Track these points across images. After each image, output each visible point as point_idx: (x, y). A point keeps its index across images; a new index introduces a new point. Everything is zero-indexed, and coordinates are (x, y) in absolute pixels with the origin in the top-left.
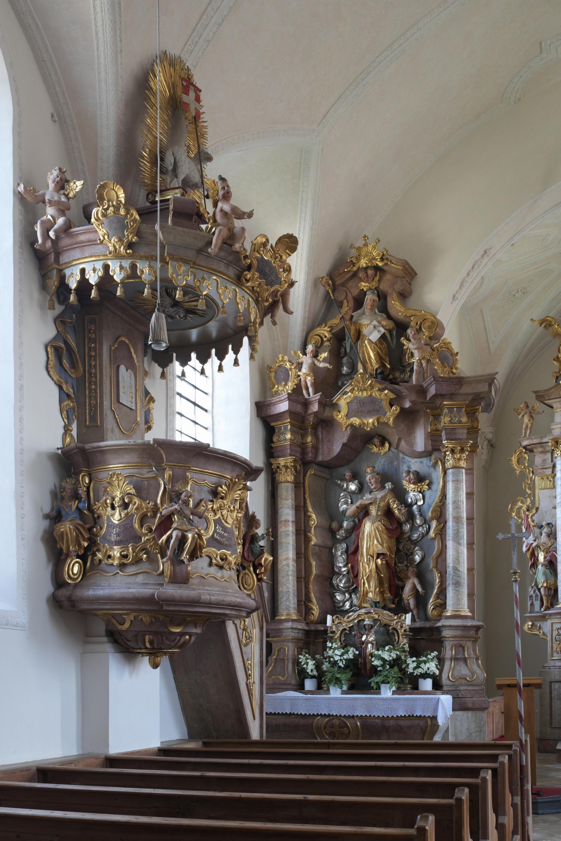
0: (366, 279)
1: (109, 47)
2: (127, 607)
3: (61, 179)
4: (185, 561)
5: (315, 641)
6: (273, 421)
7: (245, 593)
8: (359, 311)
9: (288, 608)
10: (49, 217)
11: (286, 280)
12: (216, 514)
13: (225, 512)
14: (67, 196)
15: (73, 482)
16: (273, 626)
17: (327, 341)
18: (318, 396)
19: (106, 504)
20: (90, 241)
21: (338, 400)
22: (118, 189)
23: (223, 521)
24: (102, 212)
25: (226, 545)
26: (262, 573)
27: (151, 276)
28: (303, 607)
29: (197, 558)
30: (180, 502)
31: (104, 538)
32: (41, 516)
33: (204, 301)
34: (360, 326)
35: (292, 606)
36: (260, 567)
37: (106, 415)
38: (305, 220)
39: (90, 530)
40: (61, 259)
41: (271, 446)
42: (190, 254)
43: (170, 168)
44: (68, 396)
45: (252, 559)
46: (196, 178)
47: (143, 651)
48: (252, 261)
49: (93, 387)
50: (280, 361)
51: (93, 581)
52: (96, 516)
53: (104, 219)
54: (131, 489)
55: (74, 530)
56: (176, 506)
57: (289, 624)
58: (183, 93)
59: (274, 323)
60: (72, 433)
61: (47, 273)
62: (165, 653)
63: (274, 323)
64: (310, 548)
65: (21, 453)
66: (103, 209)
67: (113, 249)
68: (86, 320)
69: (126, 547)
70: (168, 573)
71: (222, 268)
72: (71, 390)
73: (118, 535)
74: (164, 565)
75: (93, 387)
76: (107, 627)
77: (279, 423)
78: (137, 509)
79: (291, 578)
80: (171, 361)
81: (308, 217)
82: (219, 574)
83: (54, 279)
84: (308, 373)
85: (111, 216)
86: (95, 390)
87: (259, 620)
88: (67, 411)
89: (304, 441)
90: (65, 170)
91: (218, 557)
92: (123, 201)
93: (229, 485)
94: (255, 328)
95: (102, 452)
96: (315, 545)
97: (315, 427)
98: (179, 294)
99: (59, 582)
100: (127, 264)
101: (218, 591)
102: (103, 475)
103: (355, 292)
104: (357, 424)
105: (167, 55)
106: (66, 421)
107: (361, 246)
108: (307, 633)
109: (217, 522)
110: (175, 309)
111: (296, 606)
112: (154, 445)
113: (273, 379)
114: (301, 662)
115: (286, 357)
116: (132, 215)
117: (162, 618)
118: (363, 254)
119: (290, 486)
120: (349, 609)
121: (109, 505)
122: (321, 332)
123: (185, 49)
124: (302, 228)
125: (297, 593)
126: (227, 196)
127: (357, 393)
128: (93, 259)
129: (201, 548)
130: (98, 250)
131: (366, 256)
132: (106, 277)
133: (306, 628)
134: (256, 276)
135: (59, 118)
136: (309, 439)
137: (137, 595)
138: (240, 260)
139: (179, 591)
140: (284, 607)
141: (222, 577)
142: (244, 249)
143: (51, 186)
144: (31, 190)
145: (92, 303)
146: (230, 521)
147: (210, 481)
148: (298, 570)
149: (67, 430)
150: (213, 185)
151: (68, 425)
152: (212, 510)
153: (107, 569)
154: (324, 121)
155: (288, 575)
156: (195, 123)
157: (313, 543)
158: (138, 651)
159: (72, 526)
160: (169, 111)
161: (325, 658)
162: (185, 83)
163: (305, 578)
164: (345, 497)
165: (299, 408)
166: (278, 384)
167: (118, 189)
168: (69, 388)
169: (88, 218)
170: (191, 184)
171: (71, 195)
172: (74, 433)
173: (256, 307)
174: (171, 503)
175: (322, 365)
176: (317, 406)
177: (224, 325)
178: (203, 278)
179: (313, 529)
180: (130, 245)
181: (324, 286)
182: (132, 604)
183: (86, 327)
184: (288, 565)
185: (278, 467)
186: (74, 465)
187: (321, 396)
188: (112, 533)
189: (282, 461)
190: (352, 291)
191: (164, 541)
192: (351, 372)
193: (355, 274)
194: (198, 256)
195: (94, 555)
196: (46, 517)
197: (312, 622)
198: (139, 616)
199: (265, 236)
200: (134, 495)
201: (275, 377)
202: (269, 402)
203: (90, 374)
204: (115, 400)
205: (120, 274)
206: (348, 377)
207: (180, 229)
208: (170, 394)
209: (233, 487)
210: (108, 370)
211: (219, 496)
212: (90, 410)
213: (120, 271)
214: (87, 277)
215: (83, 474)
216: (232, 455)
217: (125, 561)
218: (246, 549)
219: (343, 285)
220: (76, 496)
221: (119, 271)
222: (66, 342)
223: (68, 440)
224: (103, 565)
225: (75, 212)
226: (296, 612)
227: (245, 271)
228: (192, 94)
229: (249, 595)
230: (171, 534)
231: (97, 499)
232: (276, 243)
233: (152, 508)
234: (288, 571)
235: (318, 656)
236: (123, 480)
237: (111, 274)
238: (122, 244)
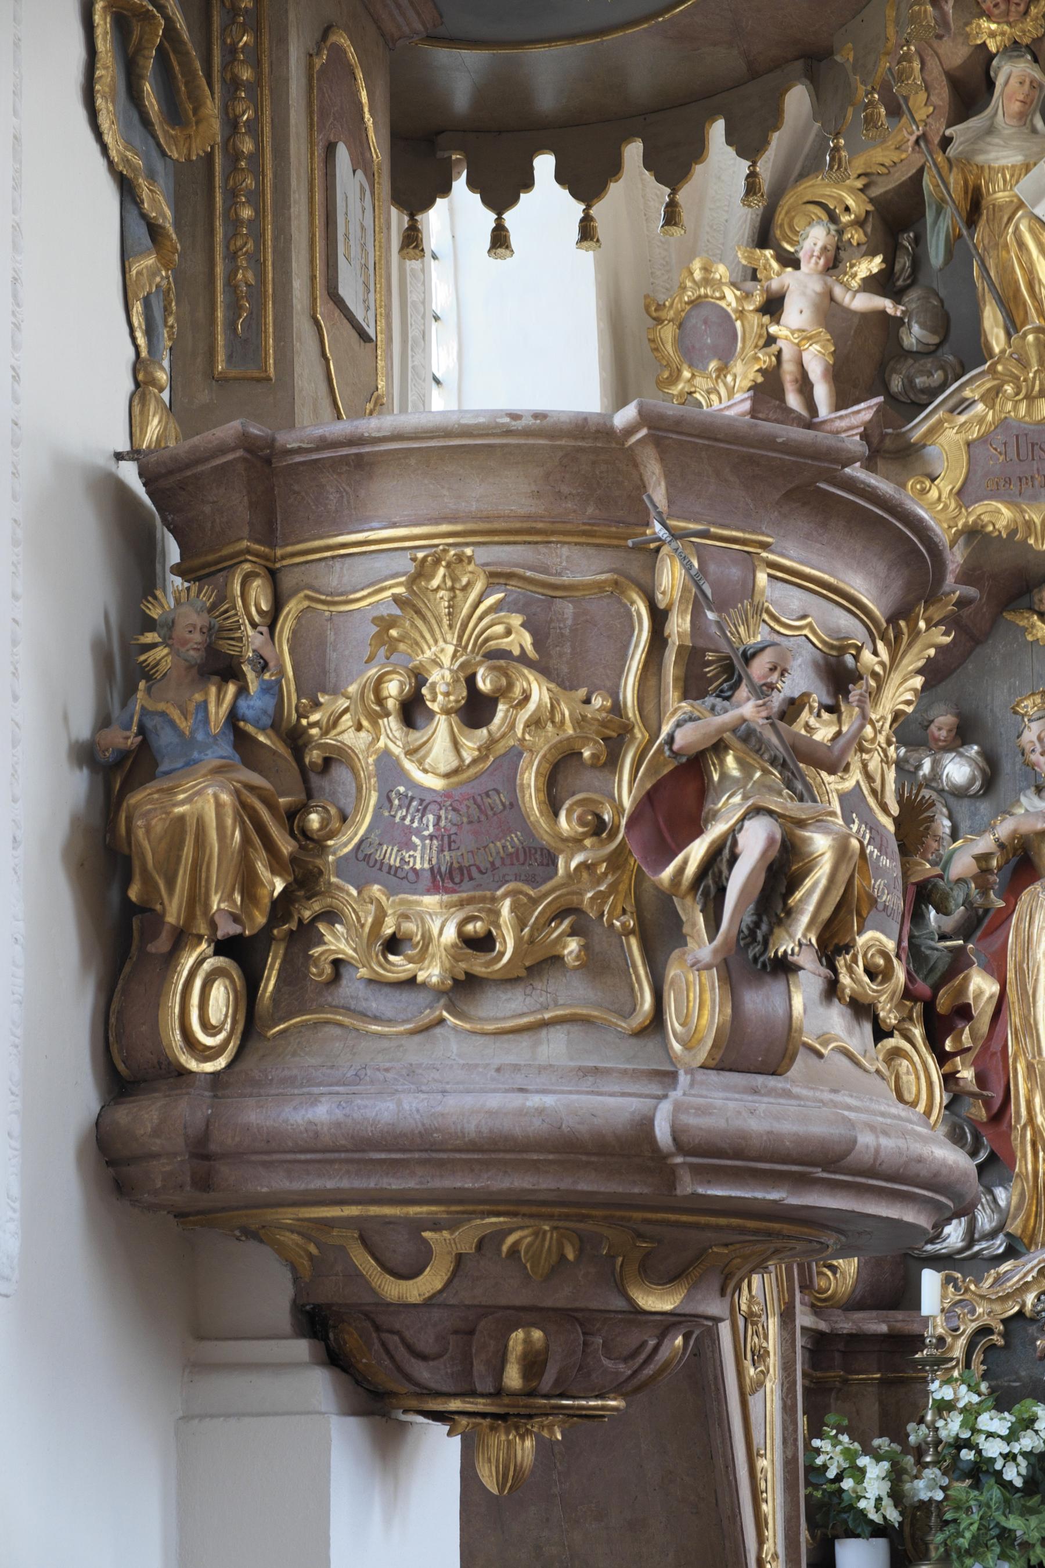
8: (974, 123)
19: (380, 701)
21: (932, 431)
39: (293, 818)
44: (154, 231)
49: (246, 213)
52: (314, 756)
69: (483, 900)
86: (256, 225)
99: (128, 1065)
103: (954, 53)
104: (1001, 524)
106: (141, 340)
113: (669, 348)
114: (825, 1467)
120: (961, 1251)
122: (828, 191)
127: (1009, 405)
137: (569, 1123)
182: (535, 1167)
187: (880, 409)
190: (941, 51)
192: (938, 346)
195: (306, 935)
198: (510, 1231)
200: (523, 659)
201: (679, 342)
206: (929, 363)
212: (234, 308)
215: (247, 567)
224: (351, 988)
233: (604, 724)
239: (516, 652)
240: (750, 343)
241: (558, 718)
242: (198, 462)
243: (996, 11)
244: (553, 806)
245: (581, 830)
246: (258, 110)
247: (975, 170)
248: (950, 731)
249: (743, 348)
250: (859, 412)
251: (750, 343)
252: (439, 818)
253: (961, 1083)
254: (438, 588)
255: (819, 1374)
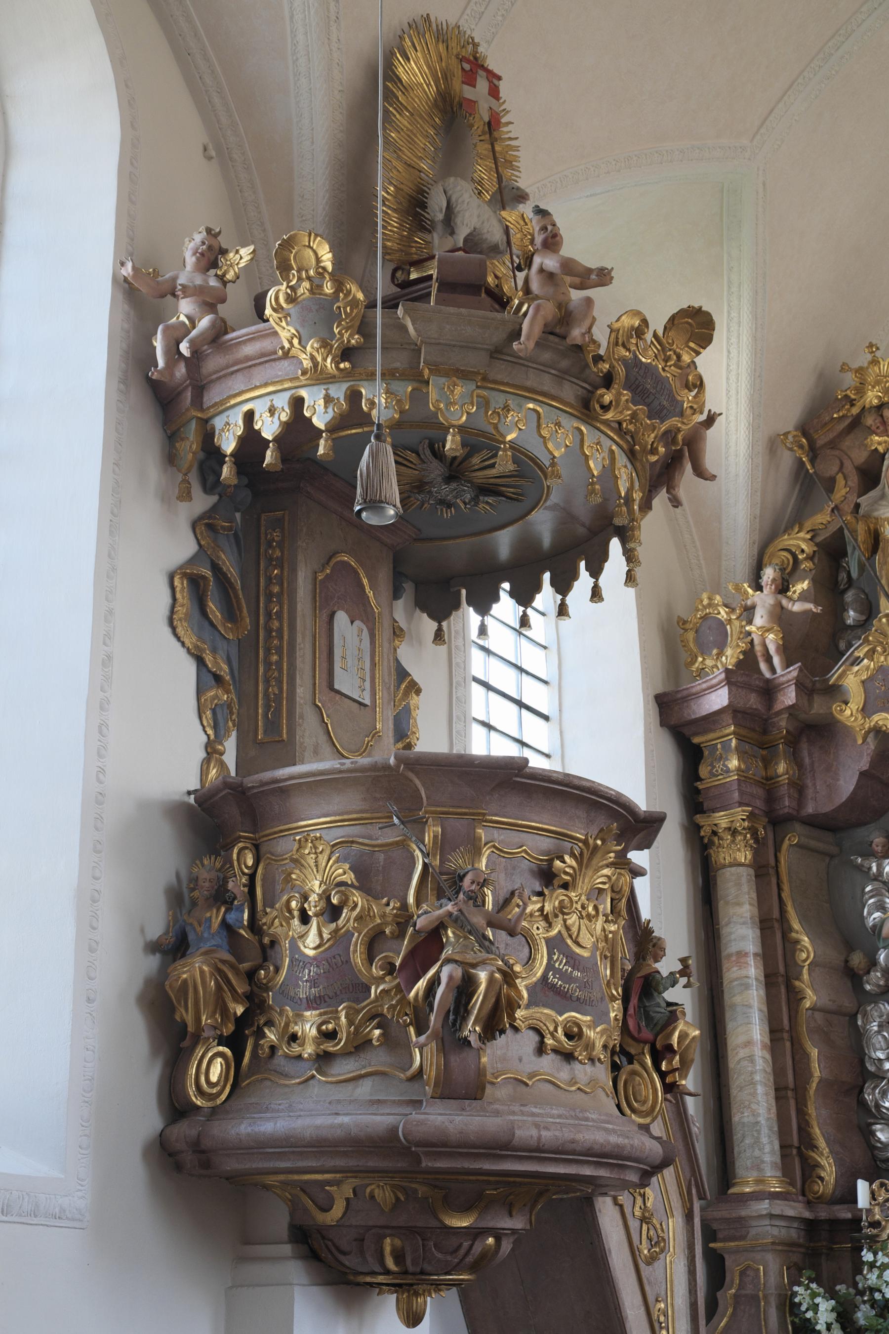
0: (882, 428)
1: (312, 13)
2: (340, 1162)
3: (210, 248)
4: (473, 1039)
5: (832, 1249)
6: (696, 734)
7: (634, 1122)
9: (758, 1166)
10: (183, 318)
11: (695, 406)
12: (550, 925)
13: (573, 919)
14: (221, 278)
15: (218, 865)
16: (723, 1212)
17: (806, 559)
18: (793, 671)
19: (290, 911)
20: (263, 355)
22: (320, 244)
23: (569, 942)
24: (287, 293)
25: (578, 999)
26: (675, 1070)
27: (391, 411)
28: (797, 1161)
29: (502, 1032)
30: (461, 896)
31: (283, 992)
32: (141, 944)
33: (509, 453)
34: (876, 524)
35: (767, 1158)
36: (669, 1056)
37: (302, 717)
38: (739, 323)
40: (205, 400)
41: (697, 788)
42: (475, 361)
43: (440, 216)
44: (218, 679)
45: (647, 1034)
46: (496, 235)
47: (380, 1279)
48: (612, 366)
49: (275, 658)
50: (705, 607)
51: (253, 1100)
52: (266, 940)
53: (290, 306)
54: (345, 873)
55: (212, 974)
56: (449, 907)
57: (764, 1206)
58: (463, 82)
59: (676, 502)
60: (224, 757)
61: (179, 429)
62: (437, 1286)
63: (676, 502)
64: (803, 1016)
65: (99, 803)
66: (288, 287)
67: (310, 364)
68: (263, 522)
69: (331, 1012)
70: (431, 1073)
71: (547, 383)
72: (225, 667)
73: (314, 983)
74: (422, 1054)
75: (275, 658)
76: (292, 1214)
77: (711, 736)
78: (359, 918)
79: (760, 1089)
80: (457, 606)
81: (746, 317)
82: (563, 1073)
83: (191, 439)
84: (768, 626)
85: (304, 300)
86: (279, 663)
87: (681, 1194)
88: (214, 711)
89: (770, 773)
90: (218, 230)
91: (560, 1030)
92: (329, 266)
93: (581, 854)
94: (631, 511)
95: (282, 790)
96: (813, 1009)
97: (793, 741)
98: (452, 441)
99: (175, 1106)
100: (339, 392)
101: (560, 1116)
102: (285, 846)
103: (860, 457)
105: (430, 22)
106: (210, 732)
107: (866, 365)
108: (811, 1226)
109: (554, 944)
110: (454, 485)
111: (779, 1161)
112: (398, 766)
113: (692, 645)
114: (800, 1304)
115: (718, 597)
116: (349, 292)
117: (422, 1191)
118: (870, 379)
119: (745, 875)
121: (296, 913)
122: (791, 542)
123: (468, 11)
124: (734, 340)
125: (780, 1127)
126: (552, 242)
127: (882, 659)
128: (271, 389)
129: (512, 1006)
130: (280, 370)
131: (878, 383)
132: (298, 425)
133: (807, 1215)
134: (624, 398)
135: (218, 152)
136: (781, 768)
138: (587, 366)
139: (458, 1119)
140: (749, 1163)
141: (573, 1082)
142: (594, 342)
143: (191, 261)
144: (149, 274)
145: (267, 475)
146: (587, 940)
147: (538, 845)
148: (778, 1072)
149: (212, 751)
150: (522, 223)
151: (214, 741)
152: (542, 914)
153: (289, 1067)
154: (762, 131)
155: (753, 1083)
156: (490, 134)
157: (808, 1004)
158: (368, 1279)
159: (209, 966)
160: (437, 120)
161: (861, 1293)
162: (467, 67)
163: (795, 1090)
164: (876, 893)
165: (753, 701)
166: (702, 654)
167: (320, 244)
168: (220, 661)
169: (261, 316)
170: (485, 246)
171: (230, 276)
172: (230, 758)
173: (629, 466)
174: (438, 899)
175: (797, 607)
176: (793, 694)
177: (566, 517)
178: (507, 408)
179: (805, 971)
180: (346, 353)
181: (791, 449)
182: (345, 1154)
183: (263, 536)
184: (751, 1059)
185: (715, 833)
186: (224, 824)
187: (801, 670)
188: (301, 978)
189: (722, 819)
190: (852, 456)
191: (421, 993)
192: (866, 621)
193: (856, 423)
194: (494, 363)
196: (153, 947)
197: (820, 1199)
199: (638, 313)
200: (352, 886)
201: (697, 640)
202: (685, 693)
203: (269, 631)
204: (324, 684)
205: (326, 412)
206: (859, 631)
207: (452, 310)
208: (457, 680)
209: (590, 859)
210: (309, 622)
211: (556, 882)
212: (267, 707)
213: (326, 407)
214: (256, 427)
215: (241, 845)
216: (584, 783)
217: (330, 1047)
218: (631, 1011)
219: (833, 444)
220: (221, 897)
221: (322, 407)
222: (216, 568)
223: (213, 772)
224: (279, 1061)
225: (237, 301)
226: (779, 1174)
227: (597, 388)
228: (482, 85)
229: (645, 1128)
230: (438, 973)
231: (270, 902)
232: (665, 328)
233: (396, 916)
234: (752, 1073)
235: (841, 1288)
236: (328, 852)
237: (307, 414)
238: (330, 352)
239: (350, 883)
240: (735, 637)
241: (372, 914)
242: (214, 795)
243: (878, 431)
244: (370, 959)
245: (382, 973)
246: (281, 607)
247: (874, 521)
248: (883, 846)
249: (731, 641)
250: (790, 672)
251: (735, 637)
252: (310, 971)
253: (681, 1088)
254: (309, 853)
255: (812, 1245)
